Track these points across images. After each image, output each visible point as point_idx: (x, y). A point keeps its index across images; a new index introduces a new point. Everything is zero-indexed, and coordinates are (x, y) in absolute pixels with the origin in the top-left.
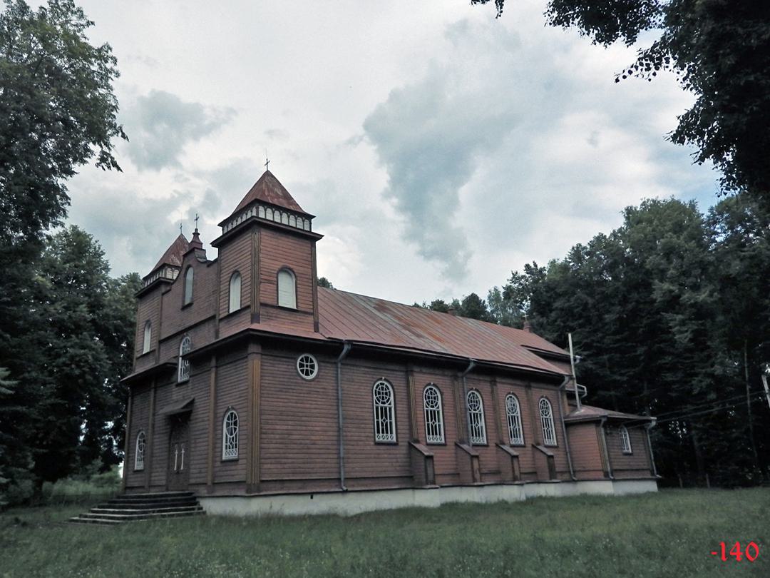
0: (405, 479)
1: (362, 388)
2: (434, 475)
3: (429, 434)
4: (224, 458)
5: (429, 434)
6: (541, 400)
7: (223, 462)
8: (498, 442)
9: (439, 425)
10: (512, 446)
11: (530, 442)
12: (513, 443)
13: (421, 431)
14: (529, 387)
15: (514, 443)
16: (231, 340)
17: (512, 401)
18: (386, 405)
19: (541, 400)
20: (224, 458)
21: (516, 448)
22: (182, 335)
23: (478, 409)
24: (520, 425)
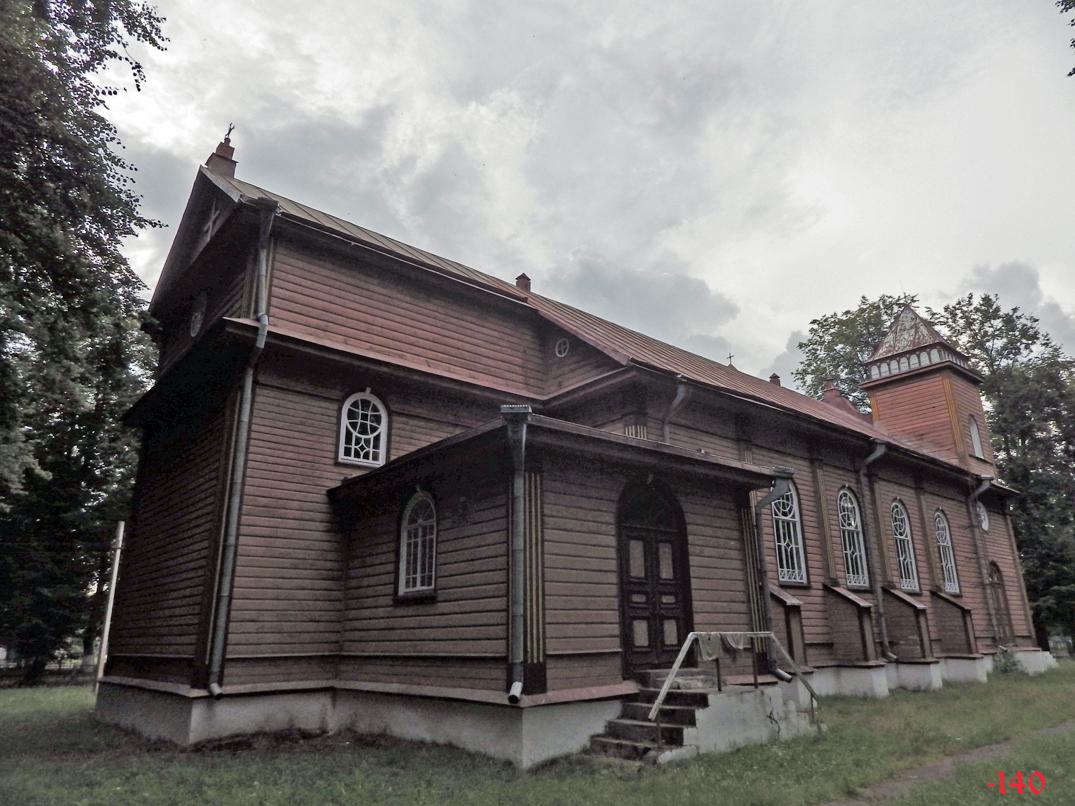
0: (304, 665)
1: (408, 428)
2: (225, 661)
3: (782, 567)
4: (402, 590)
5: (782, 567)
6: (842, 492)
7: (400, 602)
8: (934, 589)
9: (797, 549)
10: (785, 587)
11: (817, 581)
12: (853, 584)
13: (839, 572)
14: (919, 489)
15: (786, 579)
16: (422, 379)
17: (945, 519)
18: (788, 518)
19: (842, 492)
20: (402, 590)
21: (863, 595)
22: (547, 407)
23: (790, 511)
24: (912, 556)
